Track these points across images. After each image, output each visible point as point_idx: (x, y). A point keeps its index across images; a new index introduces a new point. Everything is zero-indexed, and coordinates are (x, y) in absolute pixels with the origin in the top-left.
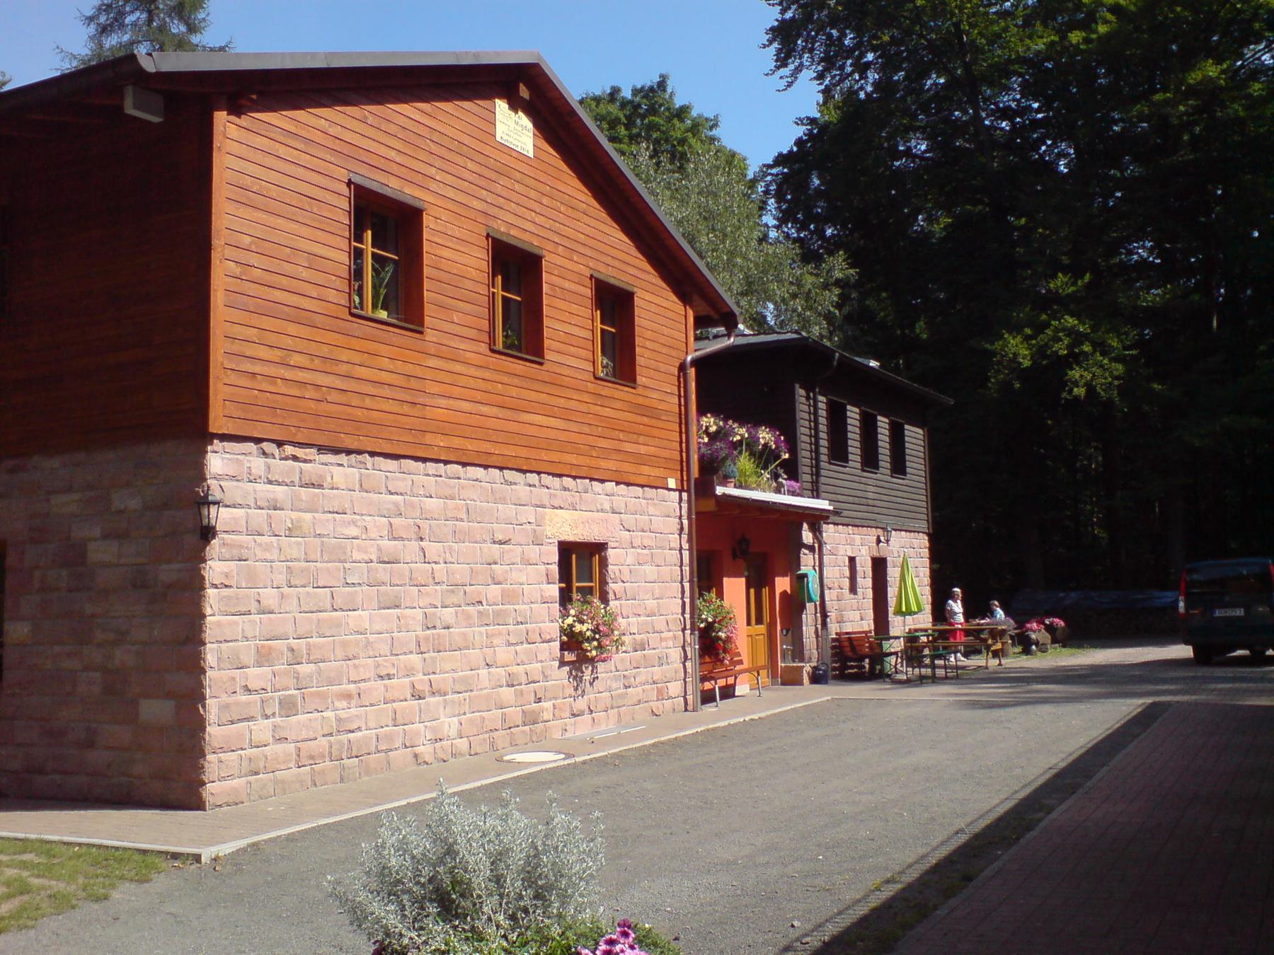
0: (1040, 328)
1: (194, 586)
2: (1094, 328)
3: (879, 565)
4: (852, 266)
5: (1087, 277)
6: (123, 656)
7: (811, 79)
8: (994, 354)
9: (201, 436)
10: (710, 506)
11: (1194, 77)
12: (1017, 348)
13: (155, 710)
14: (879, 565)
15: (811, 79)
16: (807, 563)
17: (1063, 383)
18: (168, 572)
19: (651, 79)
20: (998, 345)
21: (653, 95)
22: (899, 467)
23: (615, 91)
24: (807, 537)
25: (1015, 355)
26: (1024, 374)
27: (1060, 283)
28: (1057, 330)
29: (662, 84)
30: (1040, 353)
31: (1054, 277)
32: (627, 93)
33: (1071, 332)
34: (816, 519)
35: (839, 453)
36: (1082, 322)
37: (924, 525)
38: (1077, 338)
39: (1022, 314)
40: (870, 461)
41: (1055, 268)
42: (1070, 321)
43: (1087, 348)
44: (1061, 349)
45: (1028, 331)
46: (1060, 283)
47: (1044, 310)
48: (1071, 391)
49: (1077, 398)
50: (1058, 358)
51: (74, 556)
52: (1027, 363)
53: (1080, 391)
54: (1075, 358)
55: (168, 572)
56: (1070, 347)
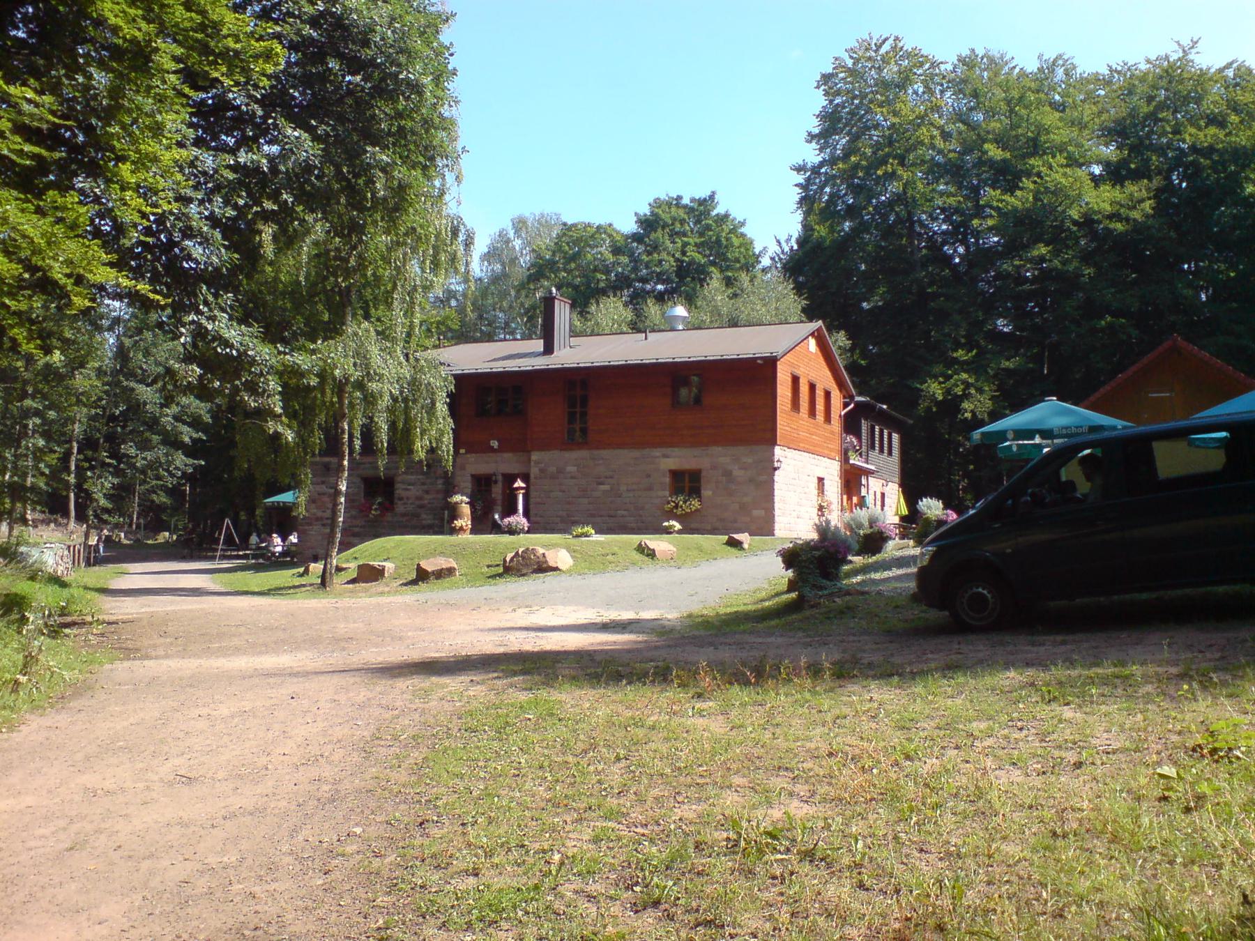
0: (948, 378)
1: (772, 482)
2: (977, 381)
3: (883, 495)
4: (848, 339)
5: (975, 351)
6: (746, 499)
7: (796, 185)
8: (922, 390)
9: (773, 442)
10: (848, 467)
11: (1035, 253)
12: (935, 389)
13: (757, 513)
14: (883, 495)
15: (796, 185)
16: (863, 492)
17: (958, 410)
18: (763, 478)
19: (702, 193)
20: (924, 387)
21: (705, 204)
22: (890, 453)
23: (679, 198)
24: (864, 481)
25: (934, 394)
26: (938, 404)
27: (960, 354)
28: (957, 380)
29: (712, 197)
30: (948, 392)
31: (957, 351)
32: (686, 201)
33: (964, 382)
34: (868, 473)
35: (873, 447)
36: (970, 377)
37: (897, 480)
38: (967, 385)
39: (938, 369)
40: (881, 451)
41: (958, 346)
42: (964, 376)
43: (973, 391)
44: (959, 391)
45: (941, 379)
46: (960, 354)
47: (949, 368)
48: (963, 415)
49: (966, 419)
50: (956, 396)
51: (728, 474)
52: (940, 398)
53: (968, 415)
54: (966, 396)
55: (763, 478)
56: (964, 390)
